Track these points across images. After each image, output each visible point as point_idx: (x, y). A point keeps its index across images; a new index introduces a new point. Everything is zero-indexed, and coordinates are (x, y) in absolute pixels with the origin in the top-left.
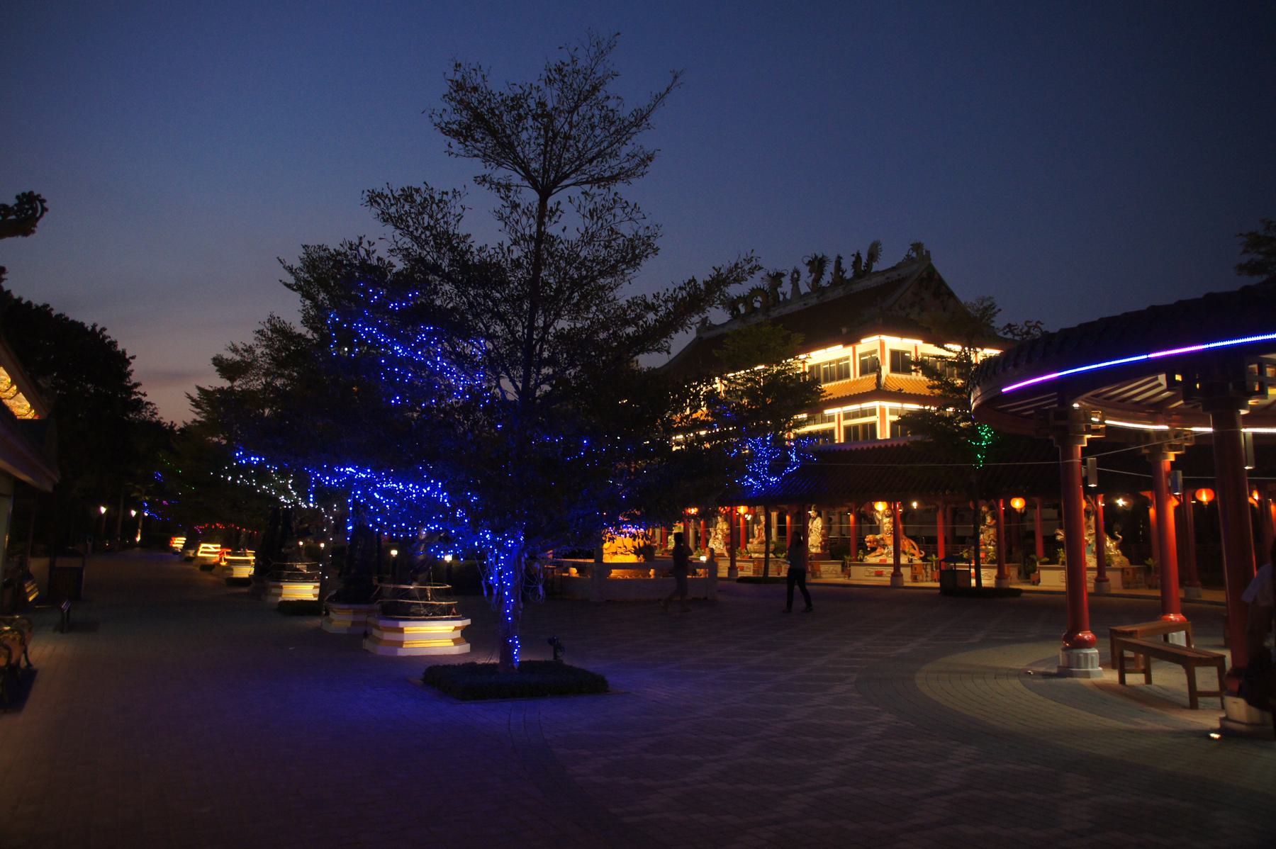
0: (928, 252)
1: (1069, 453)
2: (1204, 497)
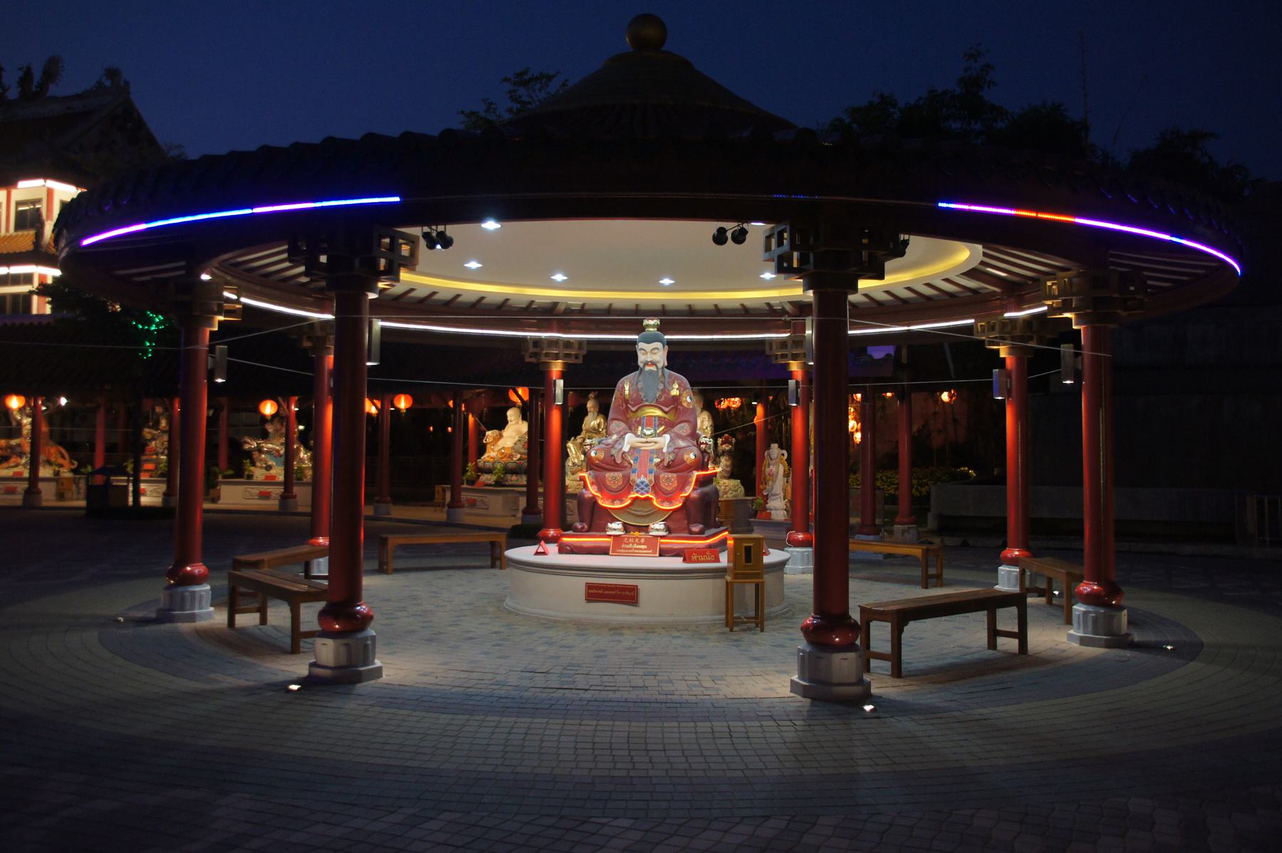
0: (127, 83)
1: (193, 337)
2: (403, 403)
